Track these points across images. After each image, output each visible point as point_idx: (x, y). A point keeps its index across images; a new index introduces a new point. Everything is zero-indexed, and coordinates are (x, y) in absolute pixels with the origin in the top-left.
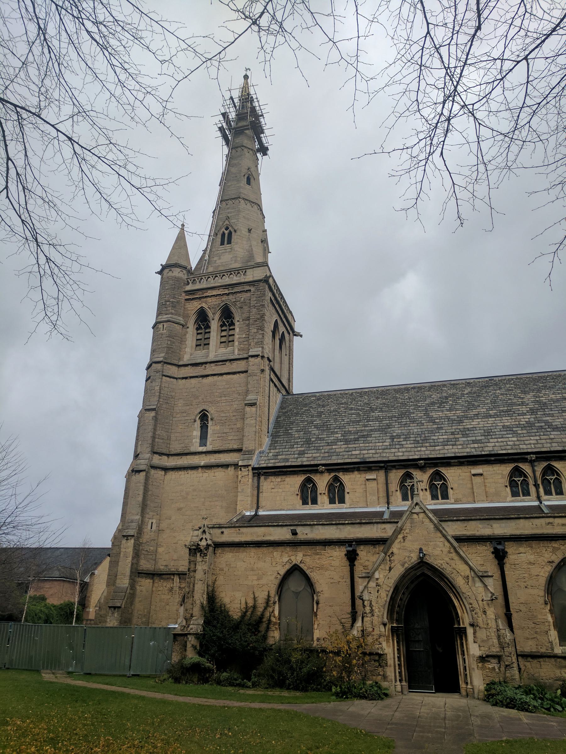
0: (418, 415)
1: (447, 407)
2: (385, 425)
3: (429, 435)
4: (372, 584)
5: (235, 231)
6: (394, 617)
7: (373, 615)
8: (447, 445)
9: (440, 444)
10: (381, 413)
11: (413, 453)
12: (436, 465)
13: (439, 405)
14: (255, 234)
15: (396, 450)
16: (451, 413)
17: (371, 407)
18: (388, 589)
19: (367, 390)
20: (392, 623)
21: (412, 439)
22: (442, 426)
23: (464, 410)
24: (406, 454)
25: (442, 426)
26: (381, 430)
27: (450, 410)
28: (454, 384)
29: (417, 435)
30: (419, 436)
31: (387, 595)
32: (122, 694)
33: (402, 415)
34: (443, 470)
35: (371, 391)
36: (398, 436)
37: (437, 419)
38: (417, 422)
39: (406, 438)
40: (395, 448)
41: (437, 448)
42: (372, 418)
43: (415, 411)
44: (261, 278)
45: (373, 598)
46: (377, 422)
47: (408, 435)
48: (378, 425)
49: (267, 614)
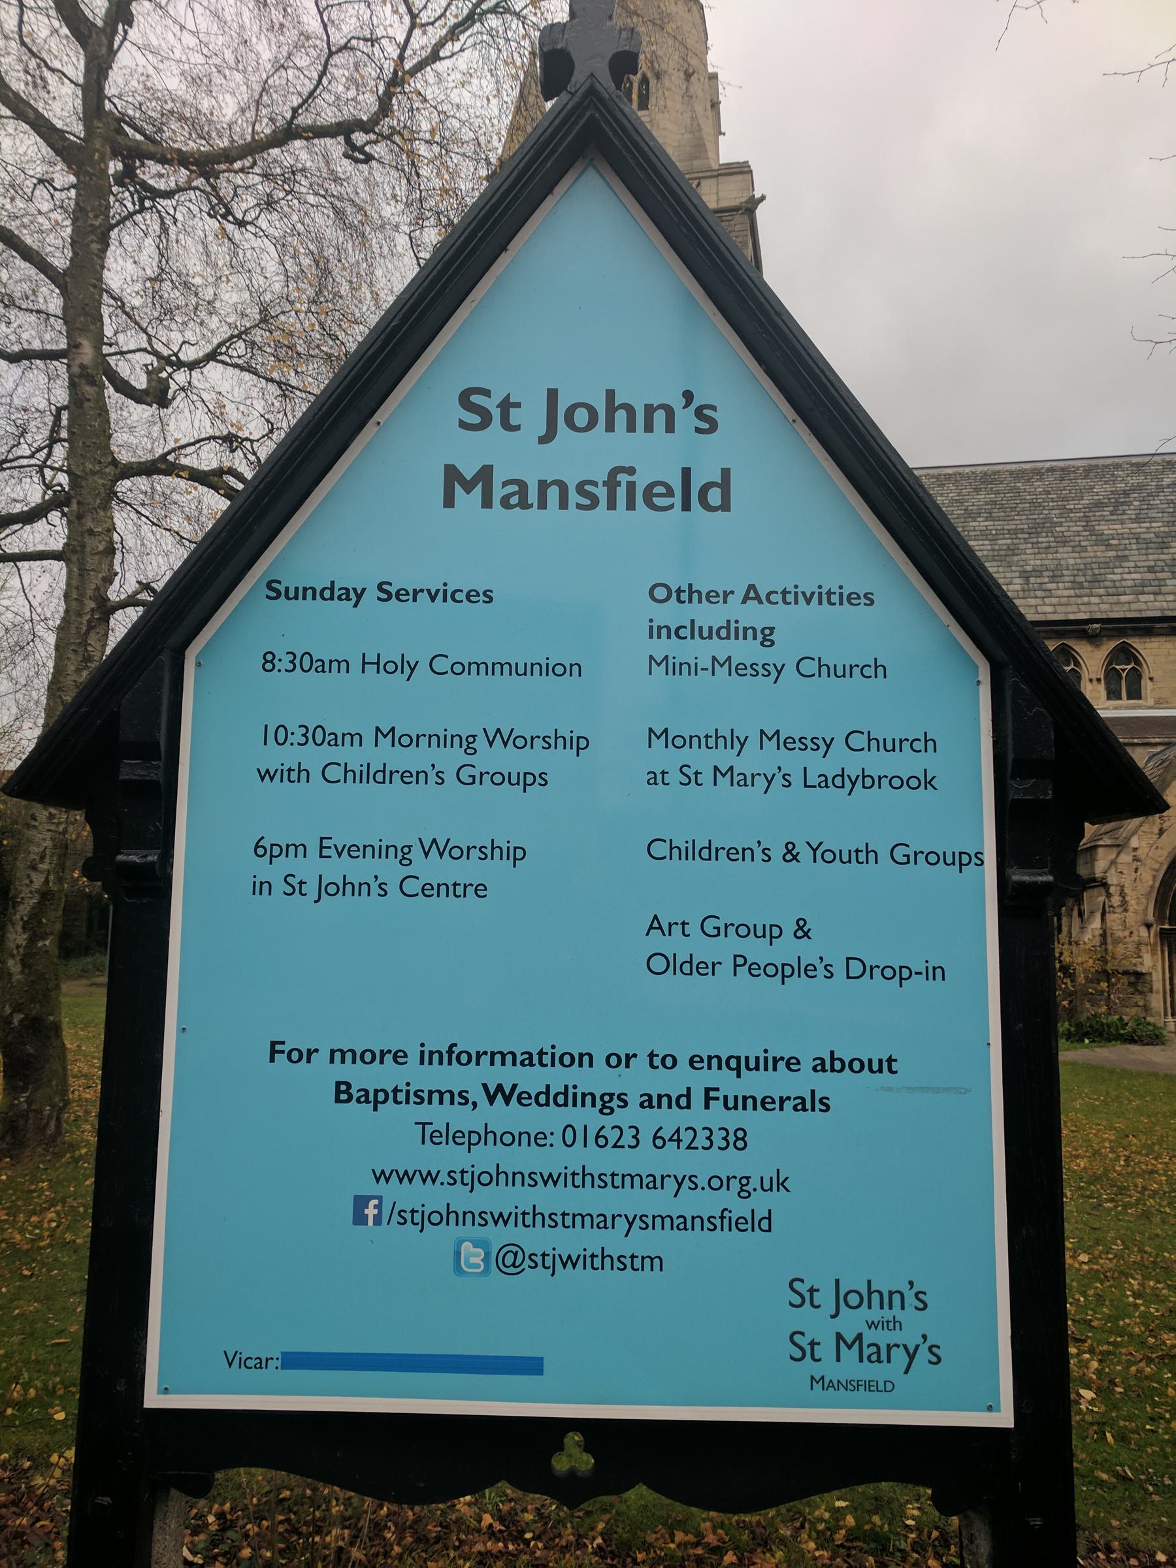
0: (1071, 529)
1: (1132, 513)
2: (1004, 547)
3: (1102, 571)
4: (1125, 858)
5: (658, 76)
6: (1165, 914)
7: (1126, 910)
8: (1143, 593)
9: (1128, 590)
10: (992, 523)
11: (1074, 608)
12: (1122, 632)
13: (1112, 508)
14: (697, 87)
15: (1039, 601)
16: (1140, 527)
17: (965, 510)
18: (1156, 866)
19: (950, 471)
20: (1163, 924)
21: (1067, 579)
22: (1127, 553)
23: (1168, 522)
24: (1059, 609)
25: (1127, 553)
26: (998, 558)
27: (1138, 520)
28: (1137, 465)
29: (1076, 572)
30: (1080, 573)
31: (1154, 877)
33: (1036, 529)
34: (1136, 643)
35: (960, 474)
36: (1038, 572)
37: (1113, 539)
38: (1072, 544)
39: (1053, 576)
40: (1036, 597)
41: (1123, 598)
42: (974, 533)
43: (1063, 520)
44: (736, 203)
45: (1127, 881)
46: (986, 542)
47: (1057, 570)
48: (989, 547)
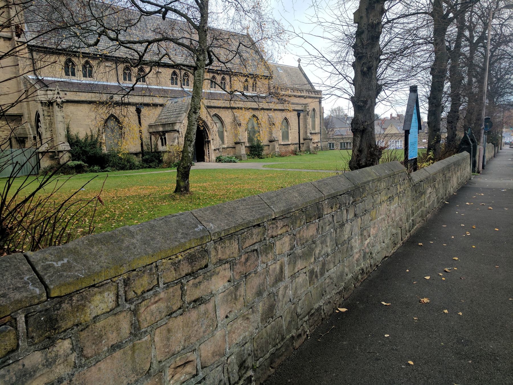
32: (132, 176)
49: (99, 139)
